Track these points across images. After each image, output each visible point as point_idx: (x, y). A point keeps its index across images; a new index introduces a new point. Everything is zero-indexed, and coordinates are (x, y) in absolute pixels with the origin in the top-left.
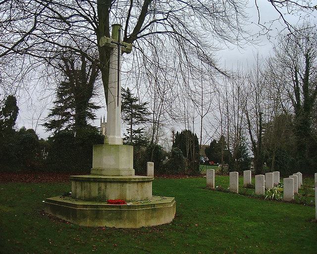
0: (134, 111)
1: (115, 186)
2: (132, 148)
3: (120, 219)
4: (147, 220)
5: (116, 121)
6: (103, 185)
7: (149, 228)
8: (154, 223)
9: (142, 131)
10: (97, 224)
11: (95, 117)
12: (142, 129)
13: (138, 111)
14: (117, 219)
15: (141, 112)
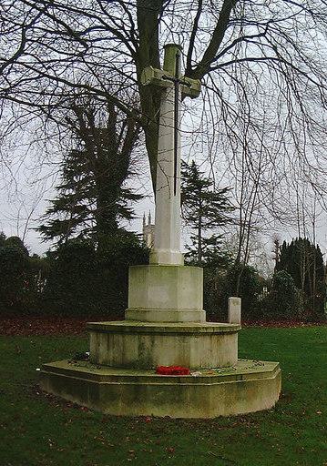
0: (204, 203)
1: (170, 341)
4: (228, 403)
6: (147, 340)
8: (241, 409)
9: (219, 240)
10: (136, 411)
11: (132, 215)
13: (212, 204)
14: (173, 401)
15: (217, 205)
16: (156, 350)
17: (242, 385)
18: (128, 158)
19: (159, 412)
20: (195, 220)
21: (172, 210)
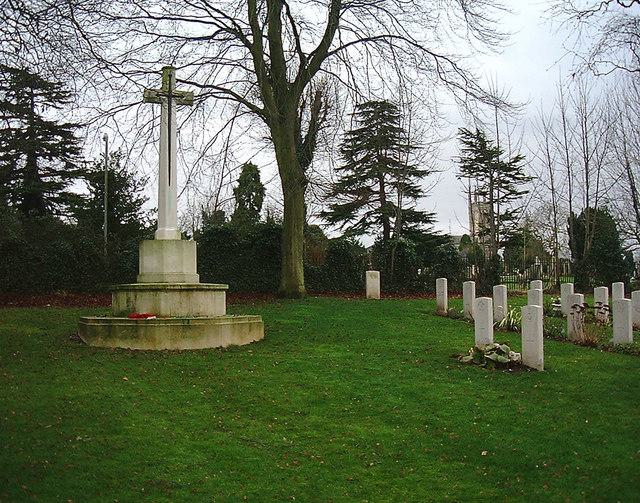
0: (495, 175)
1: (147, 295)
2: (157, 237)
3: (137, 337)
4: (174, 340)
5: (167, 207)
6: (132, 295)
7: (178, 352)
8: (186, 345)
9: (514, 215)
10: (109, 344)
11: (420, 194)
12: (514, 212)
13: (506, 175)
14: (133, 337)
15: (510, 176)
16: (138, 302)
17: (189, 327)
18: (314, 140)
19: (123, 345)
20: (484, 194)
21: (167, 198)
